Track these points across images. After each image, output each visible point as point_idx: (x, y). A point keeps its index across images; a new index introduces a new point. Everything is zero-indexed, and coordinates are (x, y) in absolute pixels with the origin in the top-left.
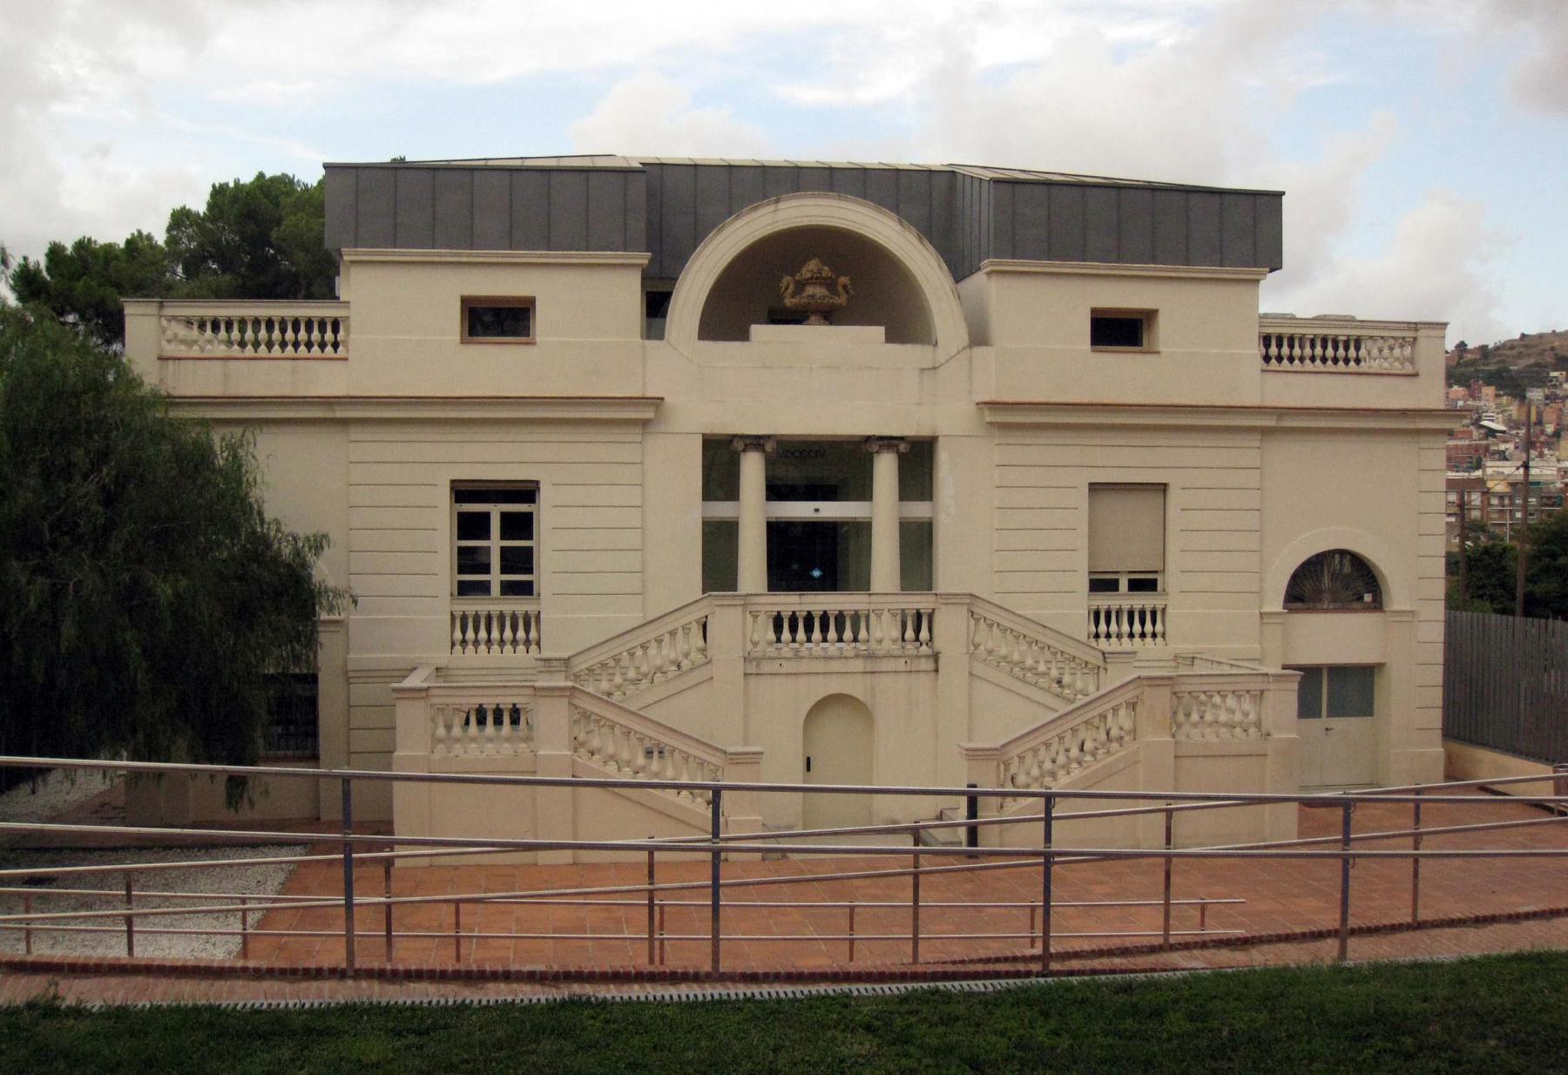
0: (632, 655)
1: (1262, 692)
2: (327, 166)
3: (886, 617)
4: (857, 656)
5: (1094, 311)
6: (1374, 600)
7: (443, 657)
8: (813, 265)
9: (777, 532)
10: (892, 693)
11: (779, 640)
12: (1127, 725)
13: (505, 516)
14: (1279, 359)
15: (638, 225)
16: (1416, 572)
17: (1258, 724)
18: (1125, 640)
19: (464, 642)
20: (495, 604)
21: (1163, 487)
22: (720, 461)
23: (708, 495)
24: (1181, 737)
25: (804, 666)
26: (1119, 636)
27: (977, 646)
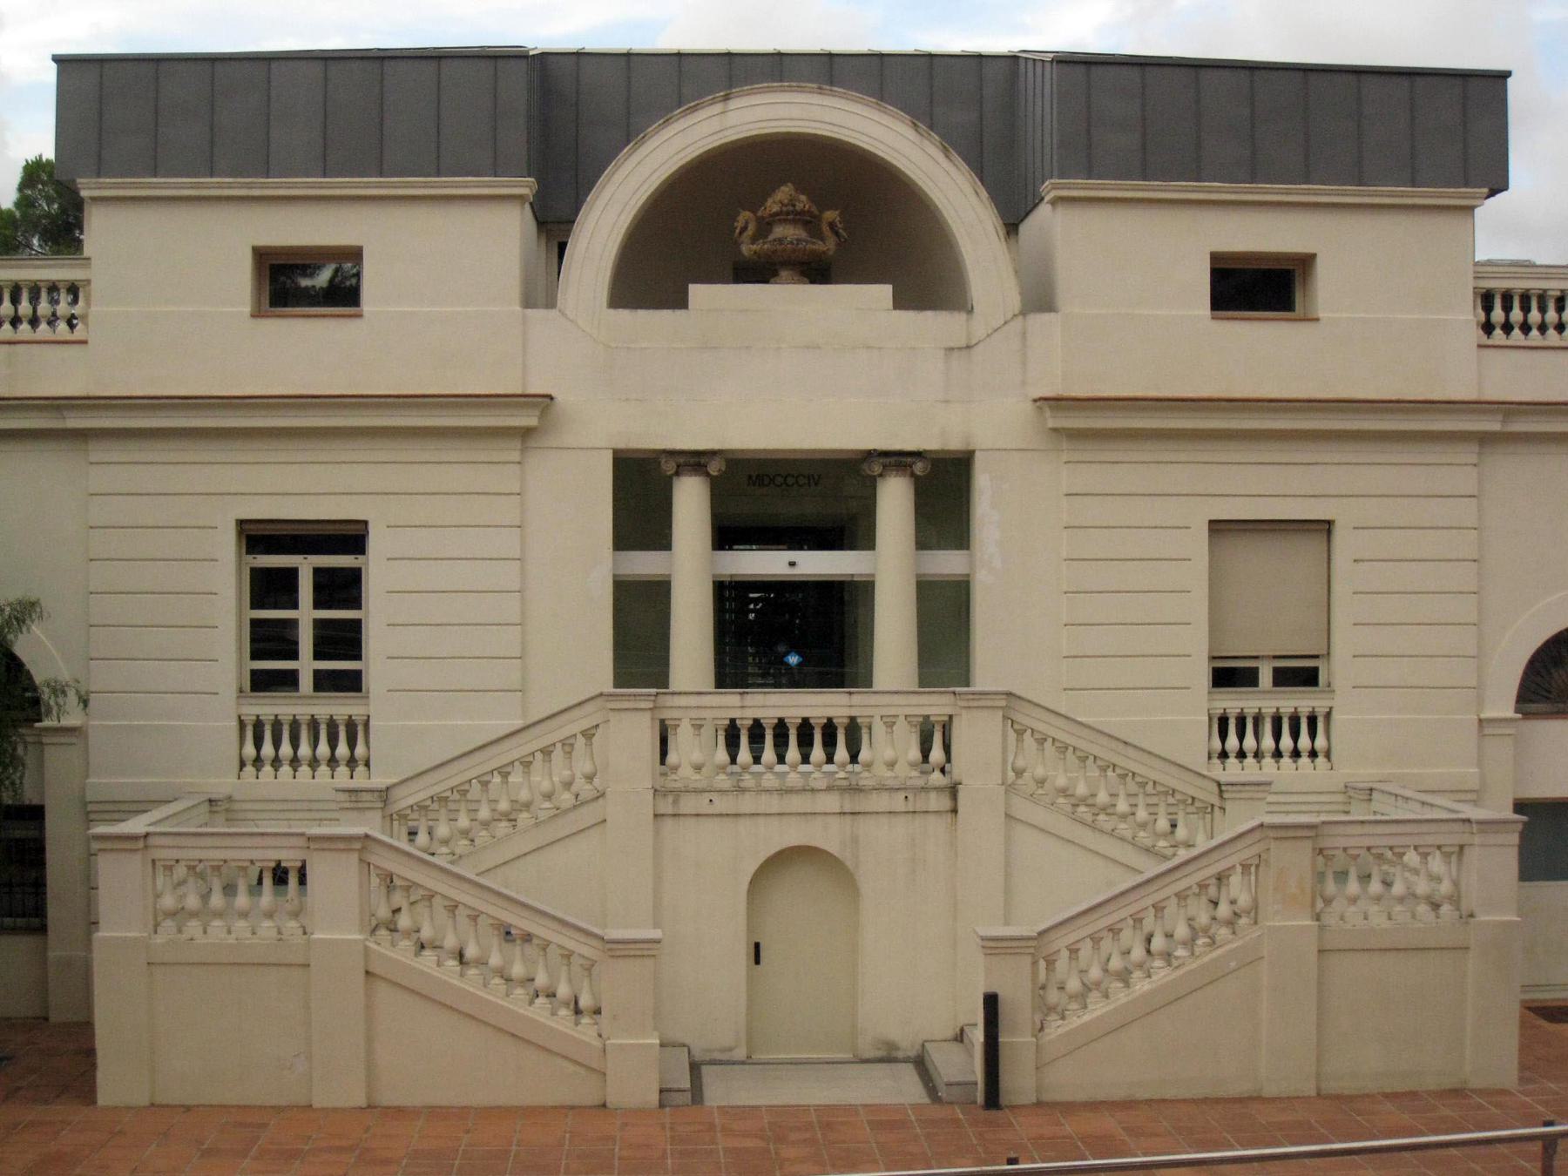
0: (485, 784)
1: (1462, 847)
2: (59, 60)
4: (829, 789)
5: (1215, 257)
7: (224, 782)
8: (784, 193)
9: (729, 594)
10: (882, 846)
12: (1244, 900)
13: (318, 572)
14: (1507, 328)
15: (515, 138)
17: (1455, 899)
18: (1268, 761)
19: (258, 762)
20: (305, 705)
21: (1325, 527)
22: (641, 493)
23: (625, 539)
24: (1330, 919)
25: (747, 804)
26: (1258, 755)
27: (1019, 773)
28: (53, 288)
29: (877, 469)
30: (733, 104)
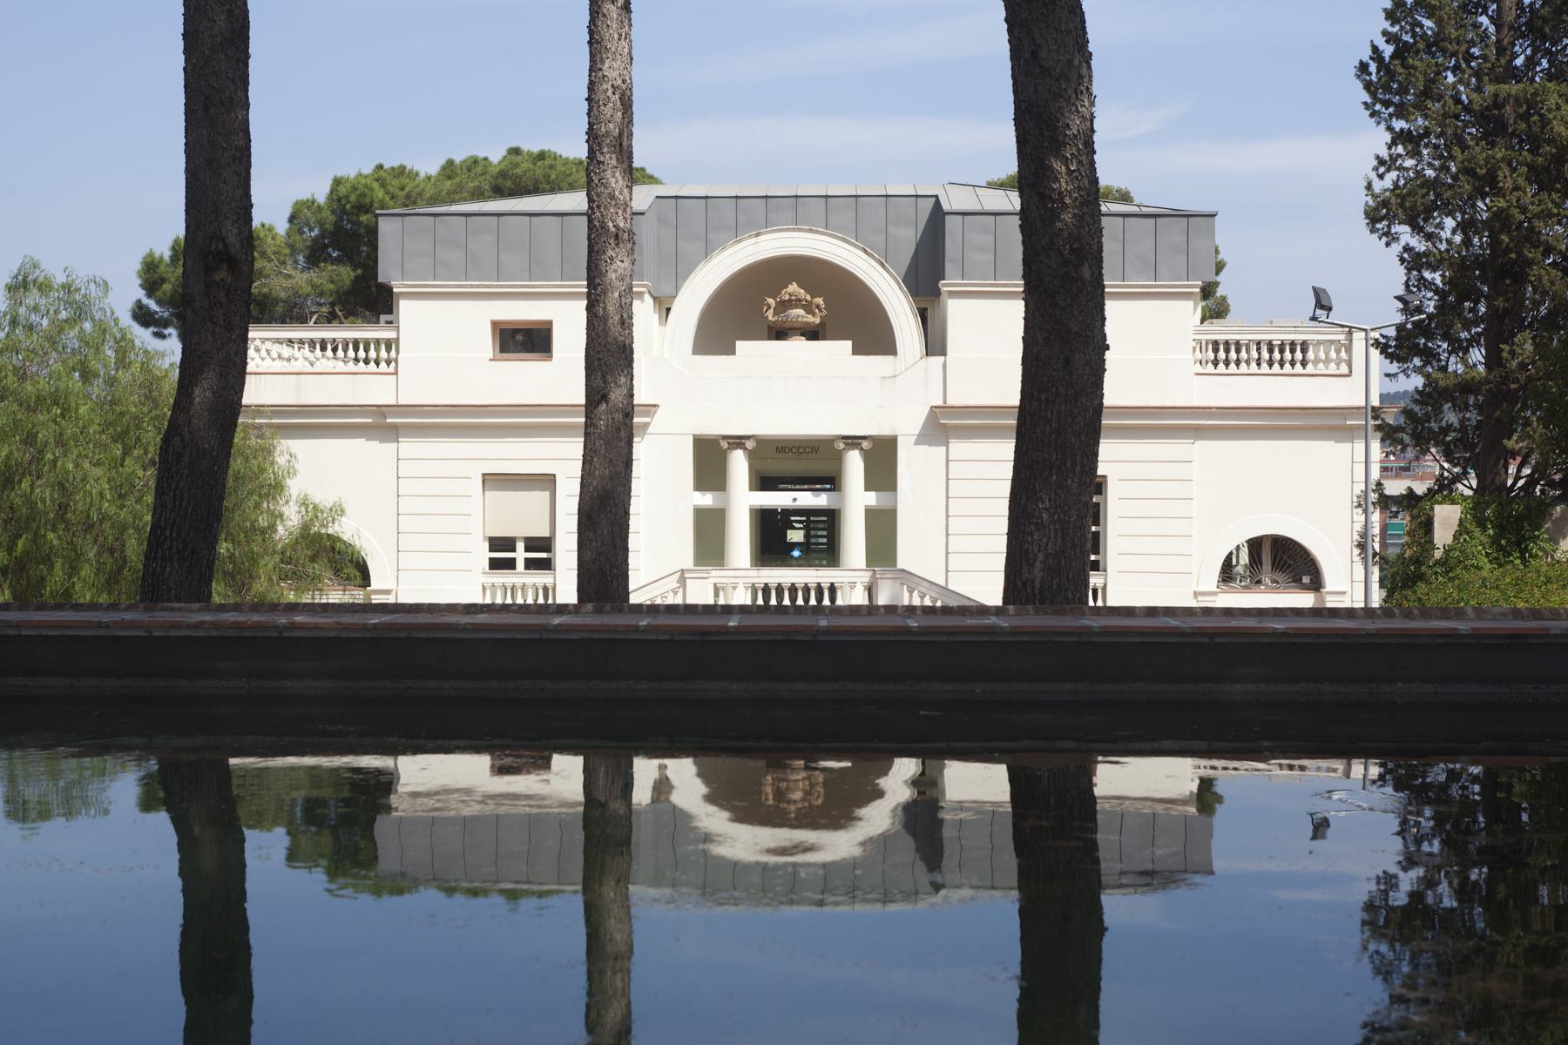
3: (741, 588)
8: (793, 288)
23: (701, 484)
28: (378, 342)
29: (842, 446)
30: (761, 238)
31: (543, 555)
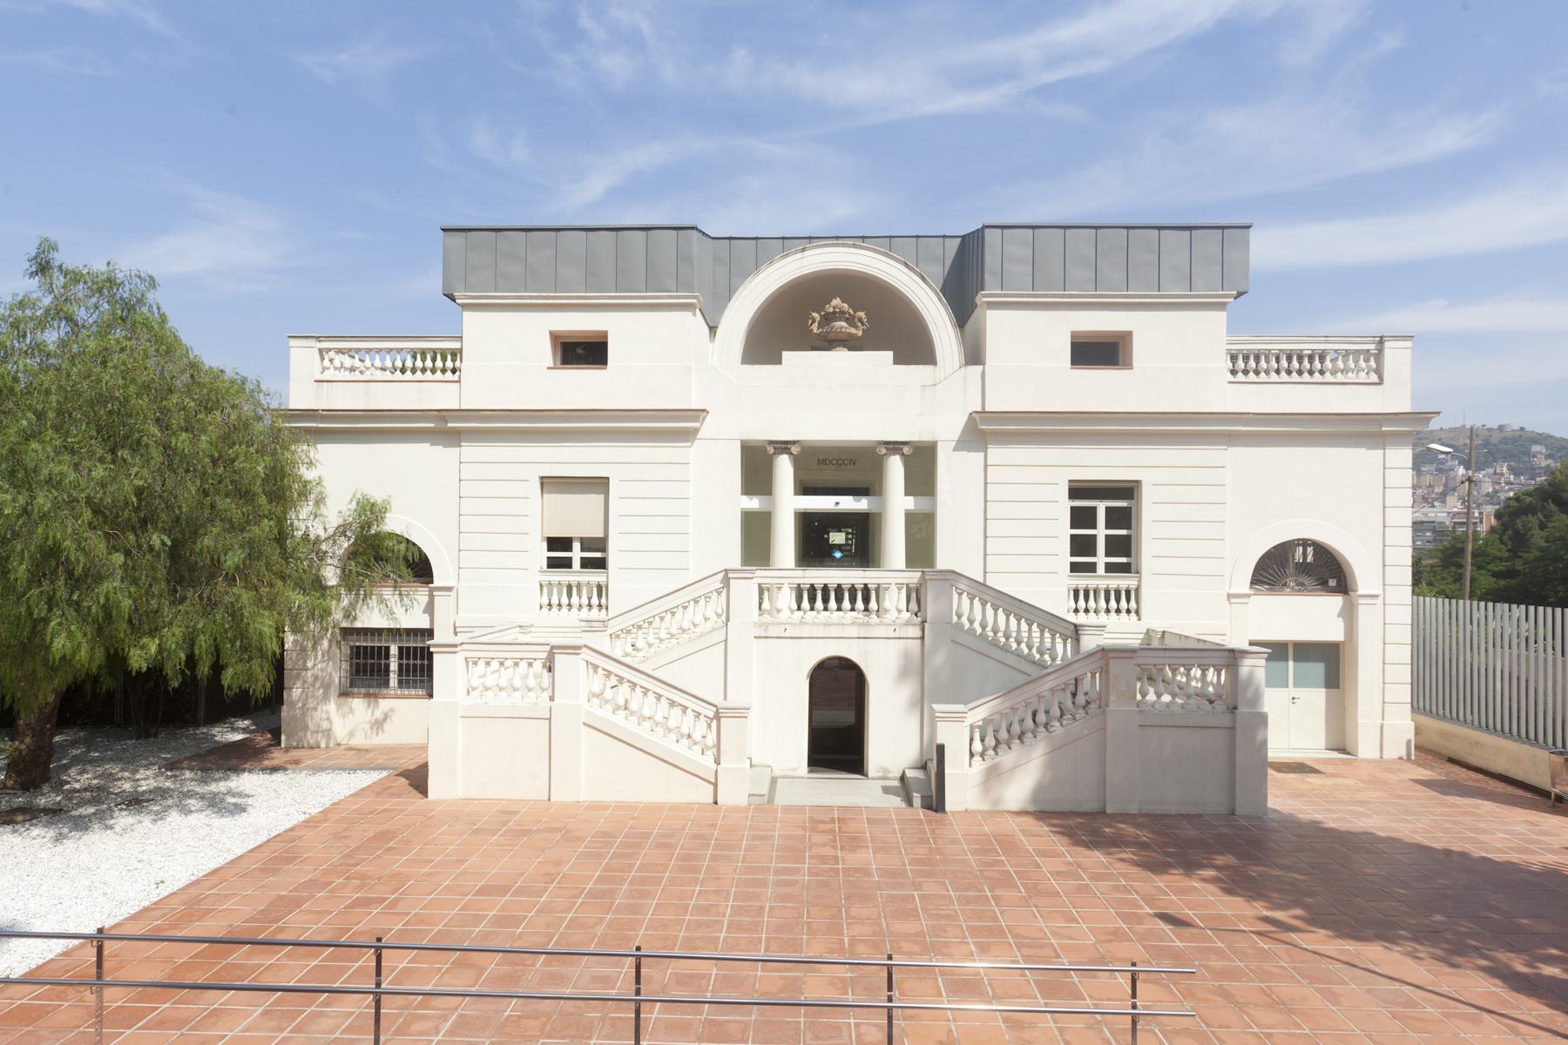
0: (662, 619)
5: (1074, 335)
6: (1339, 584)
8: (836, 302)
11: (799, 608)
13: (1108, 509)
16: (1382, 559)
18: (1103, 614)
22: (756, 466)
29: (884, 451)
30: (807, 253)
31: (1124, 560)
